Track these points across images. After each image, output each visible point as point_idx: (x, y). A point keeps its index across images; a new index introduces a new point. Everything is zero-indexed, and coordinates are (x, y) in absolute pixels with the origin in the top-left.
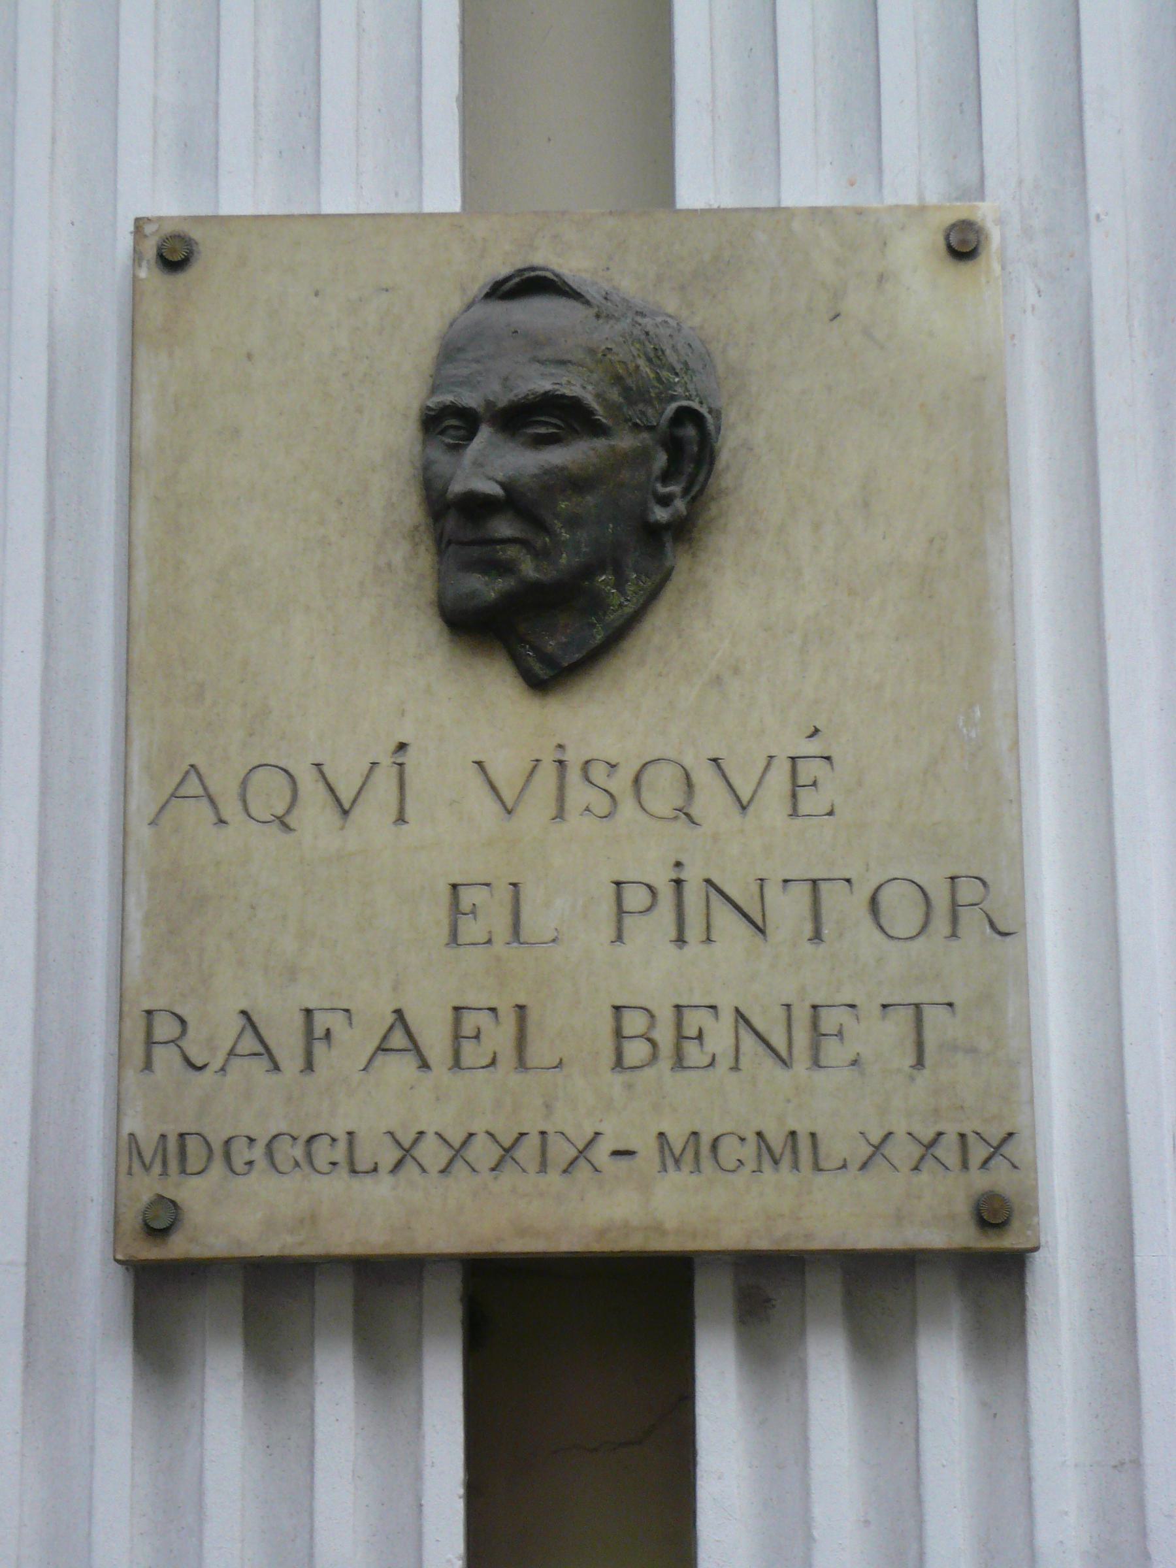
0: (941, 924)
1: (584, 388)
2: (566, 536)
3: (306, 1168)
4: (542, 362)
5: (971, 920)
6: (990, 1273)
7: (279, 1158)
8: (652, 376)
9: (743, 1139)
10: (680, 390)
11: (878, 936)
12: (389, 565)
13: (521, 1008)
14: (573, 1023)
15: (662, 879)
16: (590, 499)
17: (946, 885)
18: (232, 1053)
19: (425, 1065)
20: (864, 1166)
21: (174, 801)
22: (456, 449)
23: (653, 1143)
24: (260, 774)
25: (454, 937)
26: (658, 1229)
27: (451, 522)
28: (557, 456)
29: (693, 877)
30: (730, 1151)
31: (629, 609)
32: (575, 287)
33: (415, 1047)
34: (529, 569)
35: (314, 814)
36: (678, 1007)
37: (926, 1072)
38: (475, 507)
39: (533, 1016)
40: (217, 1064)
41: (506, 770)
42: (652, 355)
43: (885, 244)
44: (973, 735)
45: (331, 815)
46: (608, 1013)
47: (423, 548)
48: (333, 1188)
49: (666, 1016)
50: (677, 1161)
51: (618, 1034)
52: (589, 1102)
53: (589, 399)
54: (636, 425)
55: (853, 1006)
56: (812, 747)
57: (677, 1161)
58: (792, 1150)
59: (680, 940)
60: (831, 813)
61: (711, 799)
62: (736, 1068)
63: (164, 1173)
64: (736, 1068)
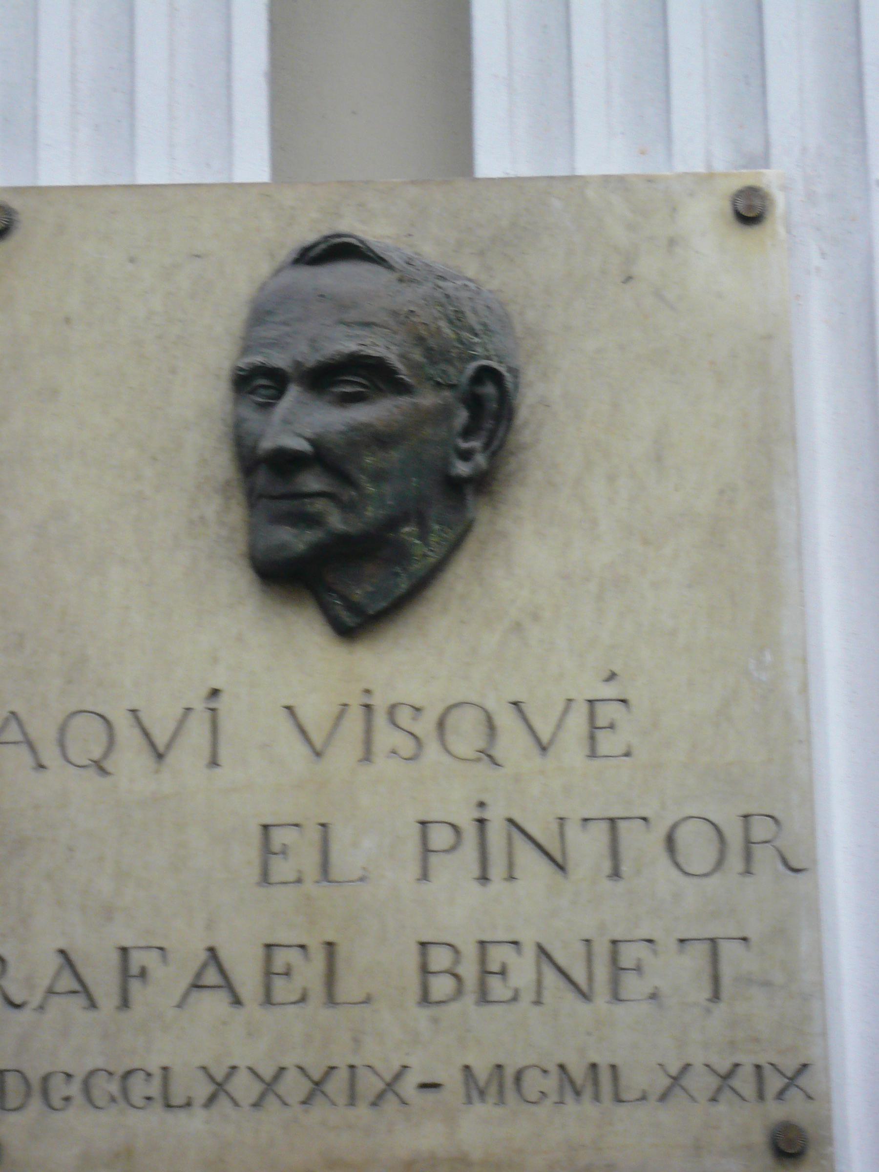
0: (735, 861)
1: (388, 348)
2: (371, 489)
3: (122, 1104)
4: (348, 324)
5: (763, 856)
7: (96, 1093)
8: (453, 336)
10: (479, 351)
11: (674, 873)
13: (330, 945)
14: (380, 960)
15: (465, 818)
16: (395, 455)
17: (739, 824)
18: (51, 991)
19: (237, 1001)
20: (664, 1097)
22: (266, 407)
25: (265, 878)
27: (262, 478)
29: (496, 816)
30: (533, 1083)
31: (433, 559)
33: (228, 984)
34: (336, 521)
35: (131, 757)
38: (285, 463)
39: (342, 952)
45: (146, 760)
46: (414, 949)
48: (147, 1123)
49: (470, 952)
51: (425, 970)
53: (393, 358)
54: (438, 384)
59: (484, 878)
60: (627, 754)
62: (538, 1002)
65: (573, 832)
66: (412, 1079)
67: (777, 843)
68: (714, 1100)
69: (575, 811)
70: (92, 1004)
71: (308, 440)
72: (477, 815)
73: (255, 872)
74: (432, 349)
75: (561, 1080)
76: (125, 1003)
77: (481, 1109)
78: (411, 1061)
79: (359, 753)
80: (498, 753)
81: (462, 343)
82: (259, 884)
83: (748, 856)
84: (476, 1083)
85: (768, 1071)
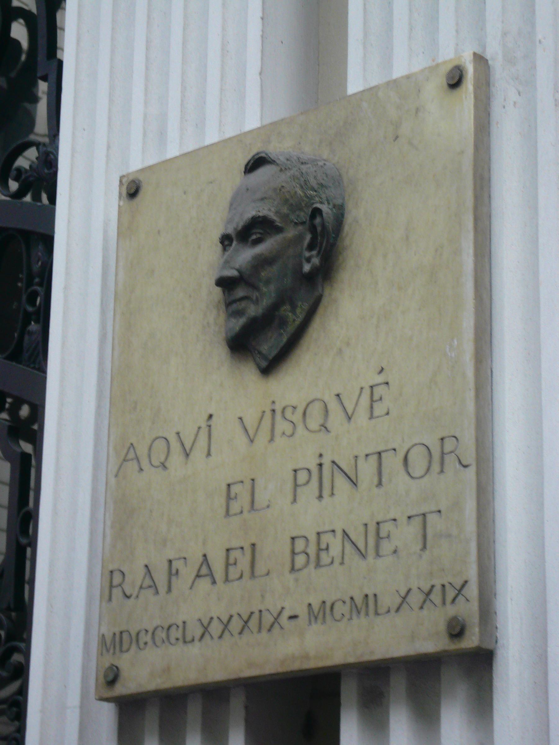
0: (436, 467)
2: (265, 289)
3: (167, 643)
5: (450, 460)
6: (477, 664)
7: (157, 638)
9: (344, 602)
11: (407, 478)
12: (208, 323)
13: (253, 545)
14: (274, 550)
15: (313, 465)
17: (438, 443)
18: (141, 587)
19: (214, 582)
20: (398, 610)
21: (125, 463)
23: (306, 609)
24: (157, 442)
25: (227, 513)
26: (307, 657)
28: (260, 249)
29: (327, 461)
30: (339, 609)
32: (273, 159)
33: (211, 574)
35: (176, 458)
36: (318, 534)
37: (427, 552)
39: (258, 547)
40: (134, 595)
41: (251, 422)
42: (303, 184)
43: (419, 91)
44: (453, 355)
45: (182, 458)
46: (289, 541)
47: (221, 312)
48: (176, 651)
49: (313, 538)
50: (316, 618)
51: (293, 553)
52: (285, 593)
53: (272, 216)
54: (296, 223)
55: (395, 520)
56: (380, 379)
57: (316, 618)
58: (365, 605)
59: (320, 497)
60: (388, 414)
61: (336, 419)
62: (342, 563)
63: (114, 653)
64: (342, 563)
65: (361, 462)
66: (286, 614)
67: (456, 452)
68: (422, 608)
69: (362, 451)
70: (157, 592)
71: (237, 270)
72: (318, 462)
73: (223, 511)
74: (292, 204)
75: (351, 606)
76: (169, 590)
77: (316, 627)
78: (287, 605)
79: (268, 438)
80: (328, 425)
81: (307, 197)
82: (225, 517)
83: (442, 463)
84: (313, 612)
85: (448, 586)
